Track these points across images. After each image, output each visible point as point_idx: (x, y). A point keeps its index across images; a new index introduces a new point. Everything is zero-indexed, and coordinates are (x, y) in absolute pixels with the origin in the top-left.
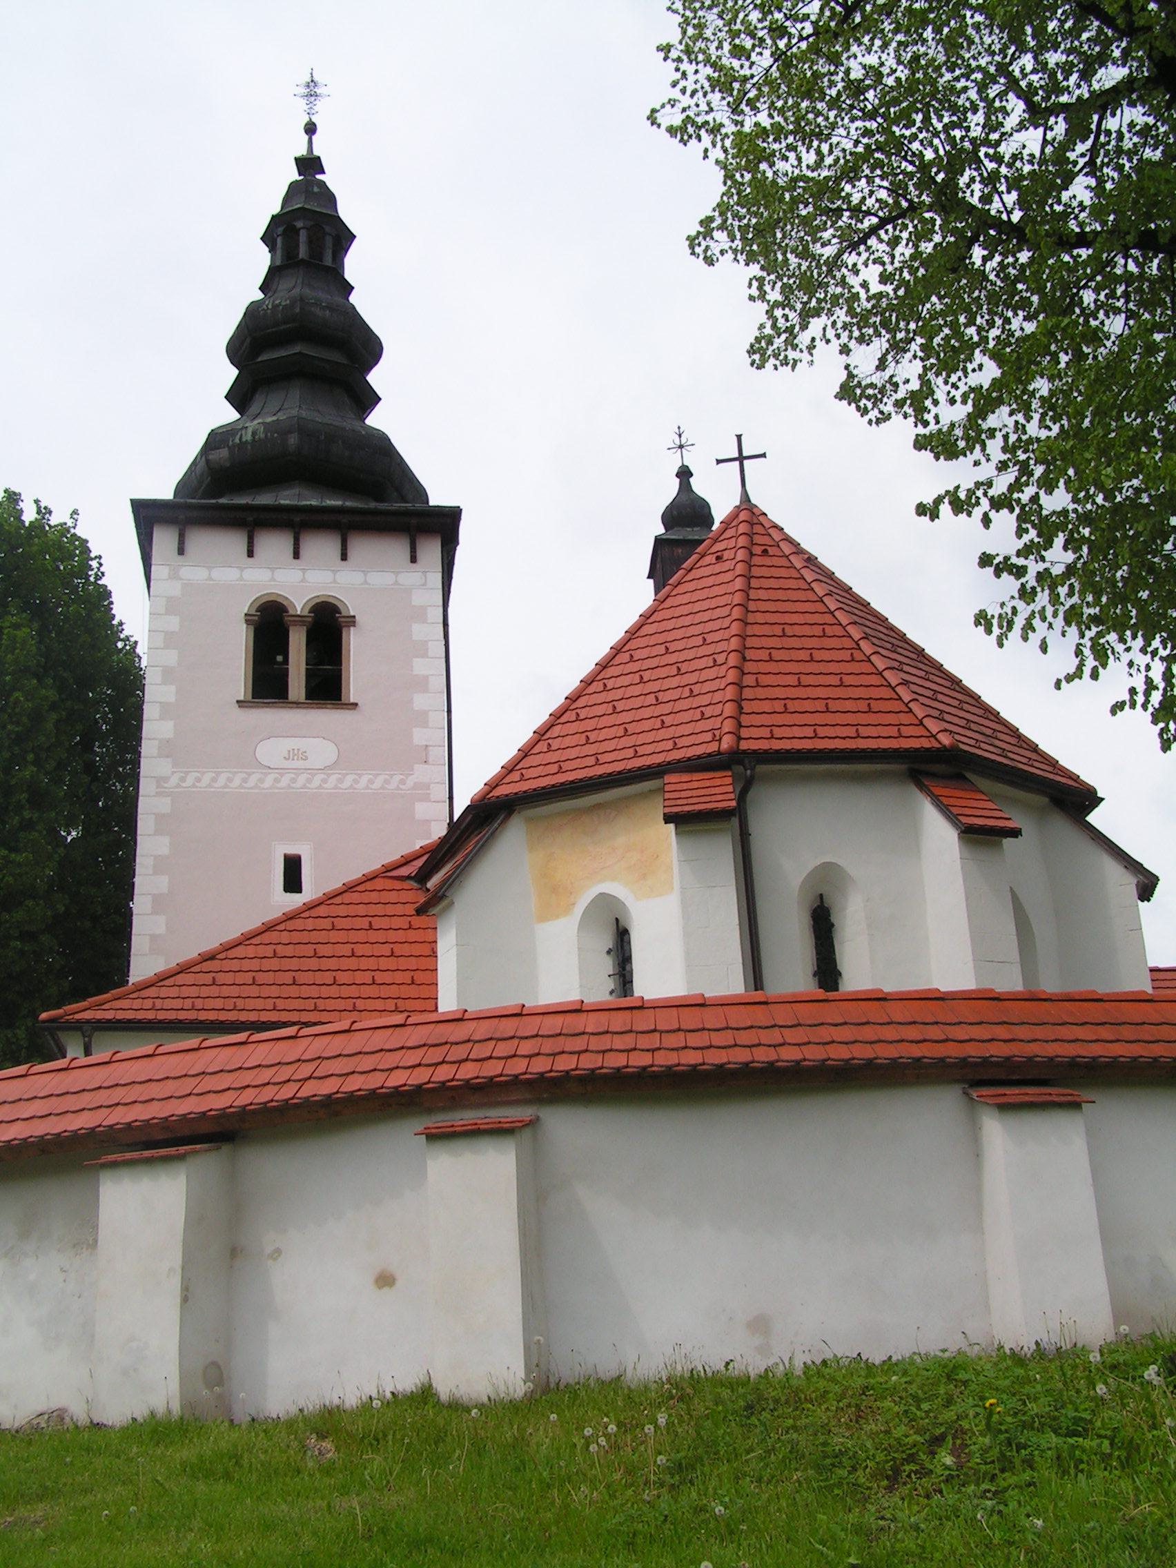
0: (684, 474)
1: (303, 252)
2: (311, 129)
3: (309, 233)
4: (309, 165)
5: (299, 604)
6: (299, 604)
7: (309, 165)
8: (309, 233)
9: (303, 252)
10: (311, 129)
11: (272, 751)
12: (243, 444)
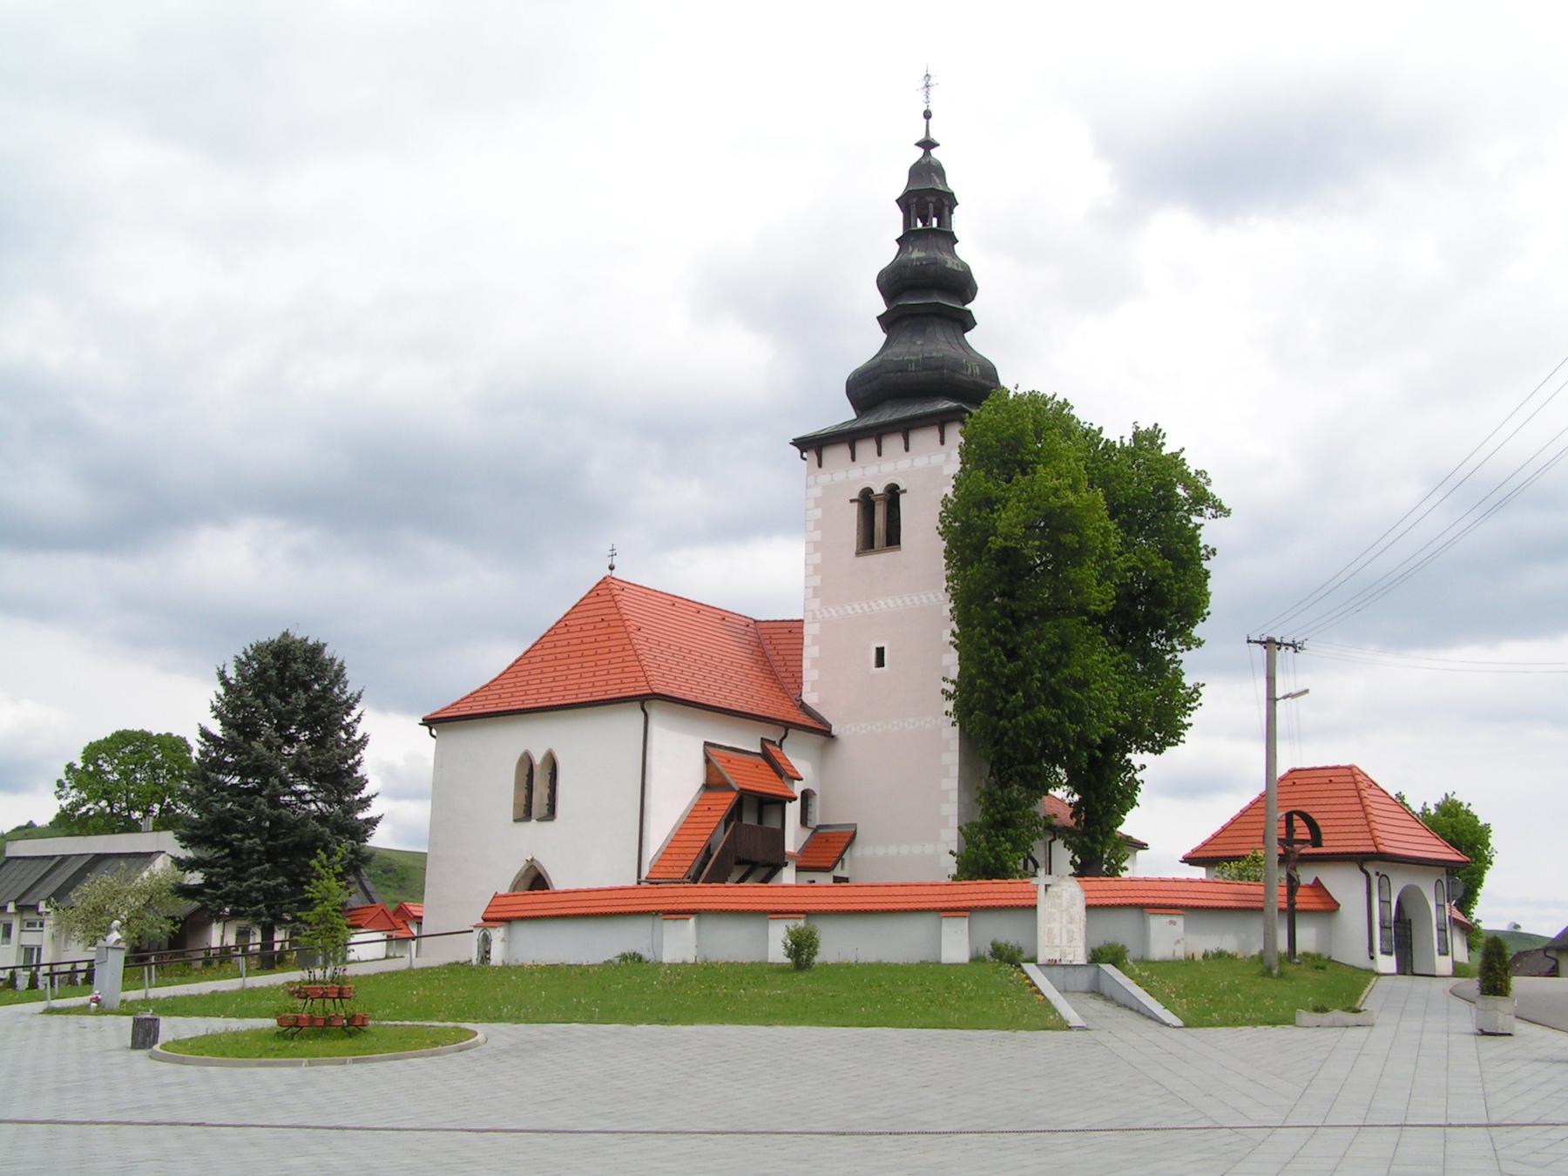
2: (927, 115)
3: (927, 201)
5: (879, 489)
6: (879, 489)
7: (927, 144)
8: (927, 201)
10: (927, 115)
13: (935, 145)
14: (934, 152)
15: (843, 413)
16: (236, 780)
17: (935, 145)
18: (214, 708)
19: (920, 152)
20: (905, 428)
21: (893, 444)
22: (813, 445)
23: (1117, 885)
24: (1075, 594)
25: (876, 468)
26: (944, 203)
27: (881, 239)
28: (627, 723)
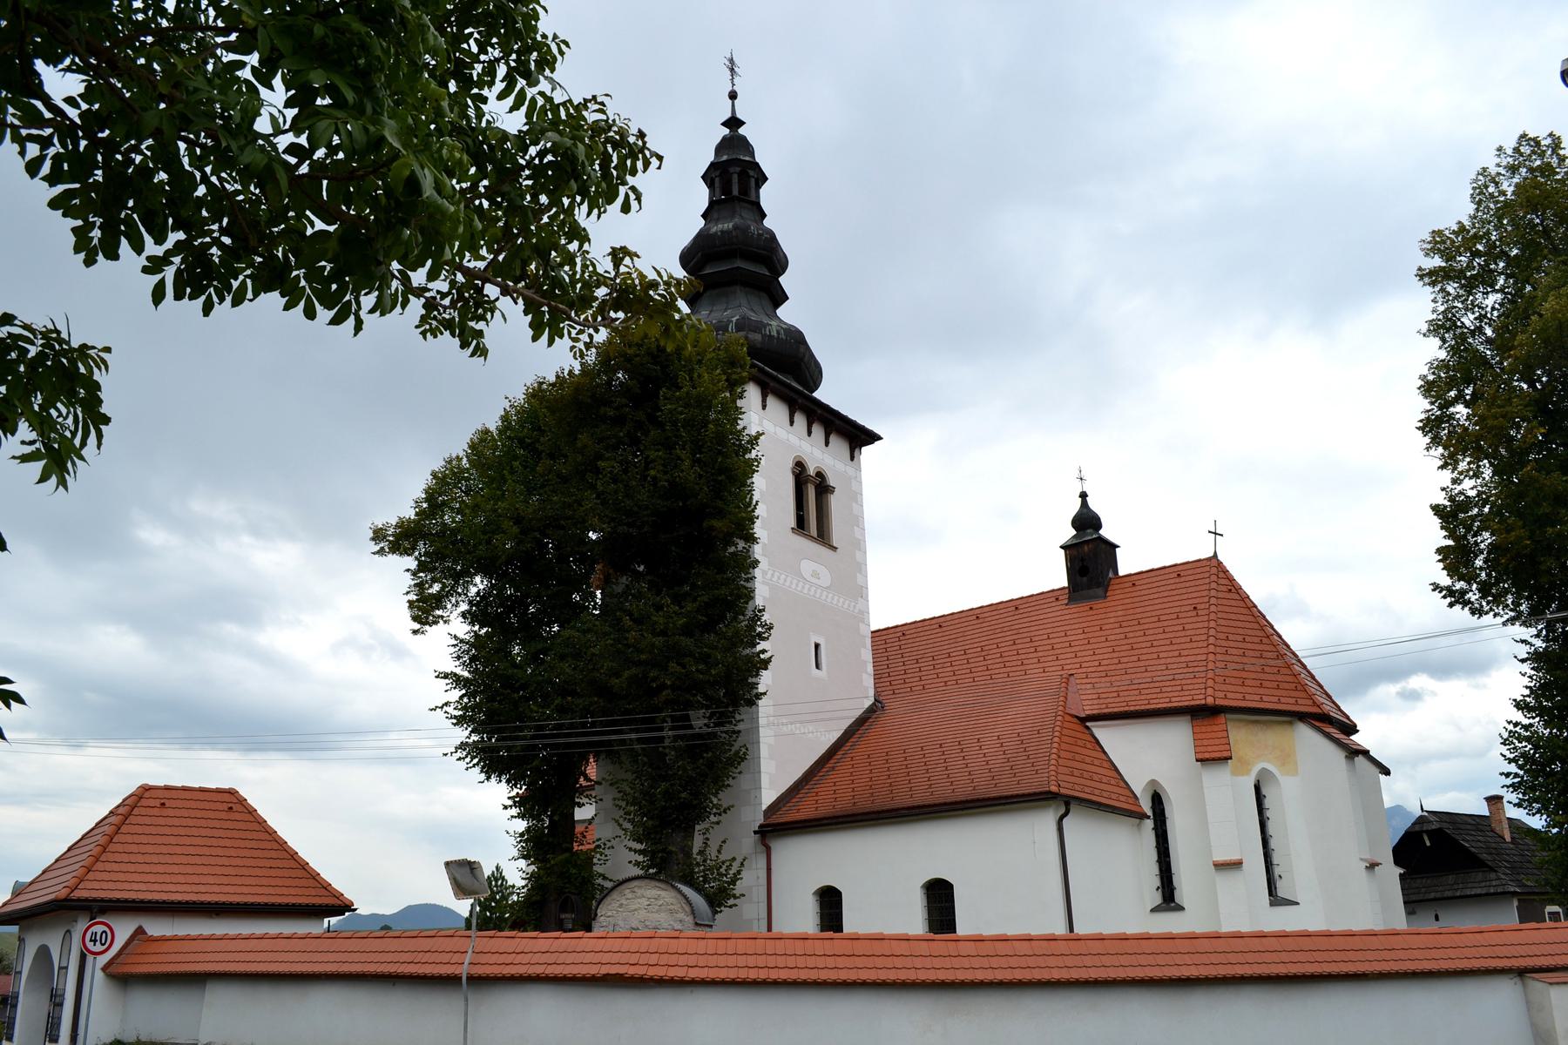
0: (1083, 496)
1: (735, 192)
2: (733, 96)
4: (733, 123)
7: (733, 123)
9: (735, 192)
10: (733, 96)
11: (807, 567)
12: (771, 336)
14: (741, 131)
19: (726, 131)
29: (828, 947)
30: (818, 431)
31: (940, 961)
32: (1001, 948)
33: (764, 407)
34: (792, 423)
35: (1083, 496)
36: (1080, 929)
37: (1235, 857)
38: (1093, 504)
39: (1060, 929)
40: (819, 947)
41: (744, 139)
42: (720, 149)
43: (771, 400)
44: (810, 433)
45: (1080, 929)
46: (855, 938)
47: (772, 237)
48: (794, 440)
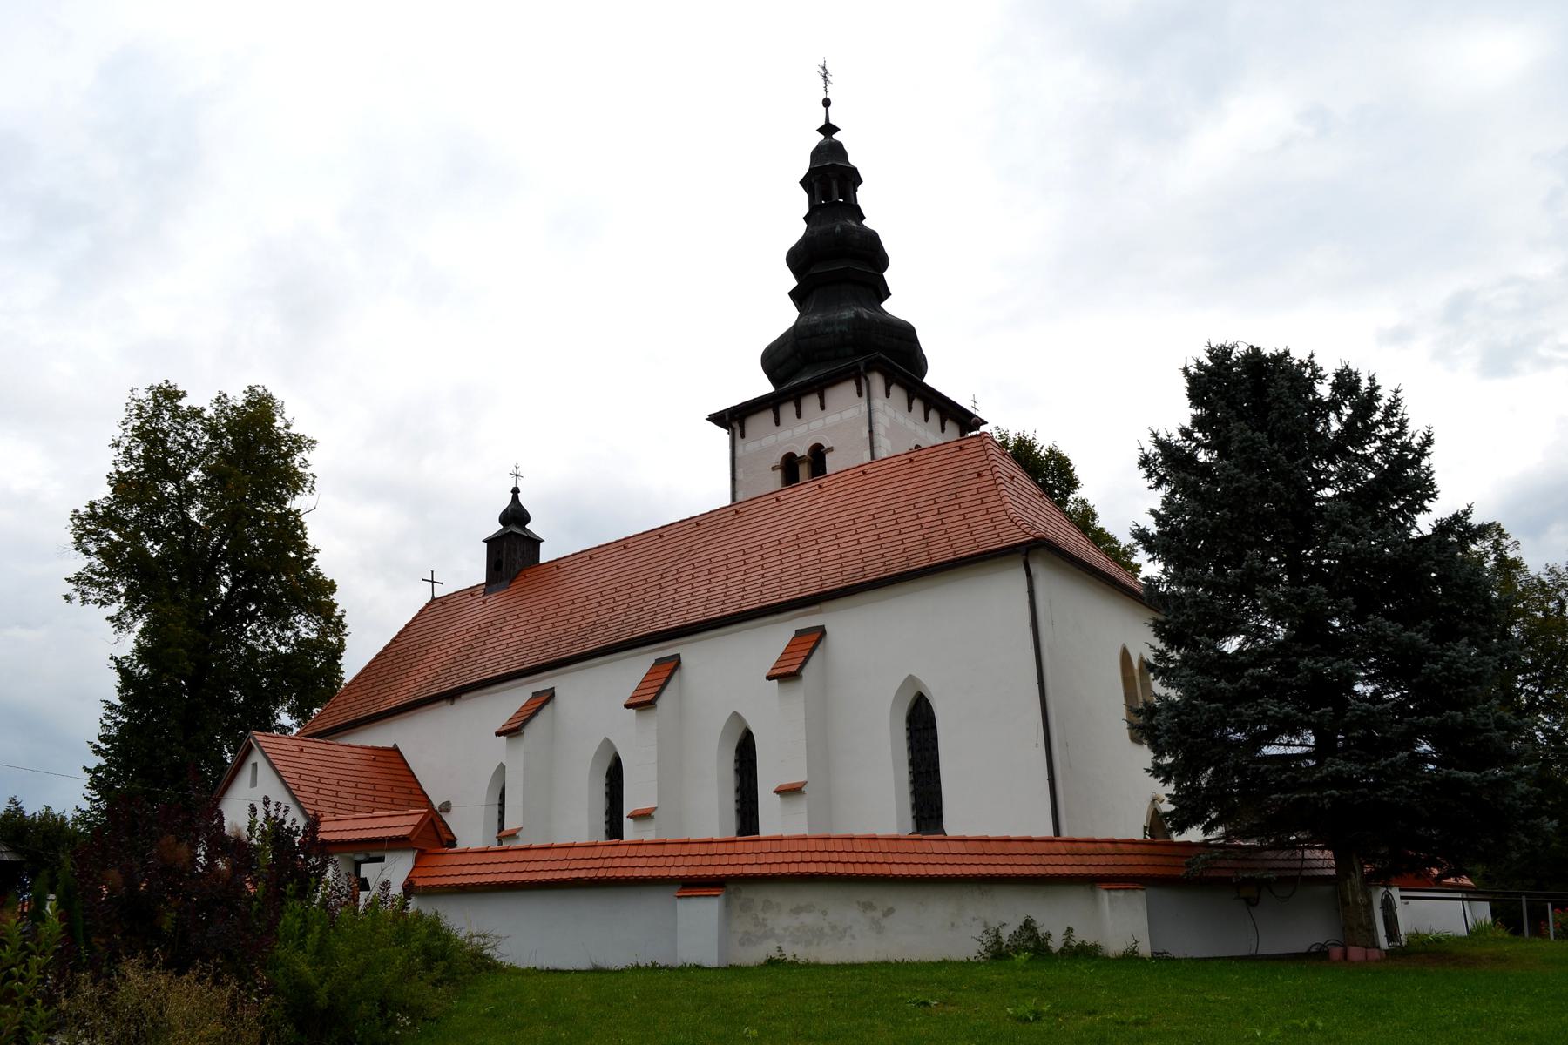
0: (516, 491)
2: (827, 103)
3: (831, 178)
4: (828, 129)
5: (802, 451)
7: (828, 129)
8: (831, 178)
10: (827, 103)
13: (837, 130)
14: (836, 137)
15: (763, 386)
16: (202, 860)
17: (837, 130)
18: (1145, 462)
19: (822, 137)
20: (819, 388)
21: (810, 403)
22: (732, 419)
23: (757, 847)
24: (1283, 416)
25: (797, 432)
26: (851, 178)
27: (789, 217)
28: (1001, 594)
29: (616, 851)
30: (934, 416)
31: (928, 859)
32: (1029, 847)
33: (888, 395)
34: (910, 409)
35: (516, 491)
36: (1065, 834)
37: (247, 810)
38: (523, 499)
39: (1049, 832)
40: (607, 852)
41: (839, 145)
42: (816, 154)
43: (894, 389)
44: (926, 420)
45: (1065, 834)
46: (465, 852)
47: (873, 238)
48: (910, 425)
